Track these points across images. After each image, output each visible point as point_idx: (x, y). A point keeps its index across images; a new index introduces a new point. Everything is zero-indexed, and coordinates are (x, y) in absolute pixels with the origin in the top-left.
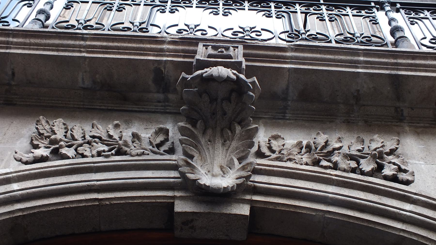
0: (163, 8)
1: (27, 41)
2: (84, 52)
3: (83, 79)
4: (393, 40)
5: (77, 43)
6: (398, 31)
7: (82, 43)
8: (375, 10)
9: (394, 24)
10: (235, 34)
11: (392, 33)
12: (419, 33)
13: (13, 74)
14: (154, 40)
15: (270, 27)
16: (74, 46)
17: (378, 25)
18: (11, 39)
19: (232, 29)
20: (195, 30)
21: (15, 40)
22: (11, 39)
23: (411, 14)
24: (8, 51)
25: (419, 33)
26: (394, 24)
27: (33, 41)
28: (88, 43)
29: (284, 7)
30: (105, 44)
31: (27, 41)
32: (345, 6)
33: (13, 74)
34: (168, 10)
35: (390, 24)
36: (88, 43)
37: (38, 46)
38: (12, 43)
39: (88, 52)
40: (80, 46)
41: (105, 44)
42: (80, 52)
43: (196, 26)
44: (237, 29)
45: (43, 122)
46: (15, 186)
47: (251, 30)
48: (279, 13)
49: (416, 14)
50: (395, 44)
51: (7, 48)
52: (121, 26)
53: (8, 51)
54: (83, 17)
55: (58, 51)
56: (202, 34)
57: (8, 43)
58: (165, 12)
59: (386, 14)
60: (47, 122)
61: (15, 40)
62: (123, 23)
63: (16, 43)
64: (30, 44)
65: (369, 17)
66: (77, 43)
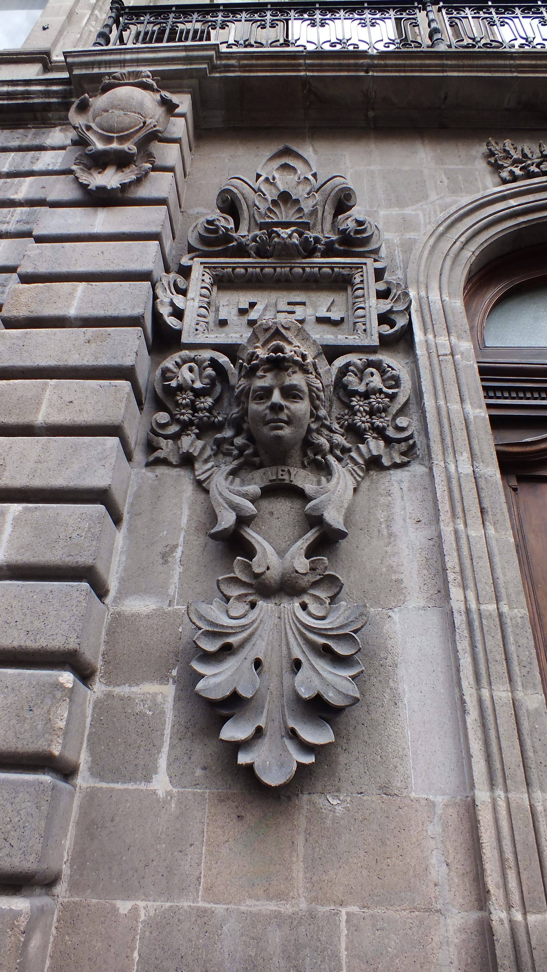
0: (263, 23)
1: (461, 62)
2: (514, 72)
3: (509, 99)
4: (430, 43)
5: (507, 62)
6: (436, 33)
7: (512, 62)
8: (417, 11)
9: (433, 25)
10: (333, 45)
11: (431, 37)
12: (518, 31)
13: (446, 98)
14: (294, 56)
15: (376, 34)
16: (505, 66)
17: (416, 28)
18: (445, 62)
19: (227, 42)
20: (348, 44)
21: (449, 62)
22: (445, 62)
23: (452, 14)
24: (445, 74)
25: (518, 31)
26: (433, 25)
27: (466, 62)
28: (518, 62)
29: (455, 13)
30: (533, 62)
31: (461, 62)
32: (464, 7)
33: (446, 98)
34: (268, 25)
35: (429, 26)
36: (518, 62)
37: (471, 68)
38: (447, 66)
39: (519, 72)
40: (511, 66)
41: (533, 62)
42: (511, 72)
43: (348, 40)
44: (334, 40)
45: (493, 143)
46: (512, 202)
47: (245, 43)
48: (373, 21)
49: (458, 13)
50: (432, 46)
51: (443, 71)
52: (278, 43)
53: (445, 74)
54: (242, 38)
55: (490, 71)
56: (354, 48)
57: (443, 66)
58: (265, 28)
59: (427, 15)
60: (497, 143)
61: (449, 62)
62: (278, 41)
63: (451, 66)
64: (463, 66)
65: (486, 18)
66: (507, 62)
